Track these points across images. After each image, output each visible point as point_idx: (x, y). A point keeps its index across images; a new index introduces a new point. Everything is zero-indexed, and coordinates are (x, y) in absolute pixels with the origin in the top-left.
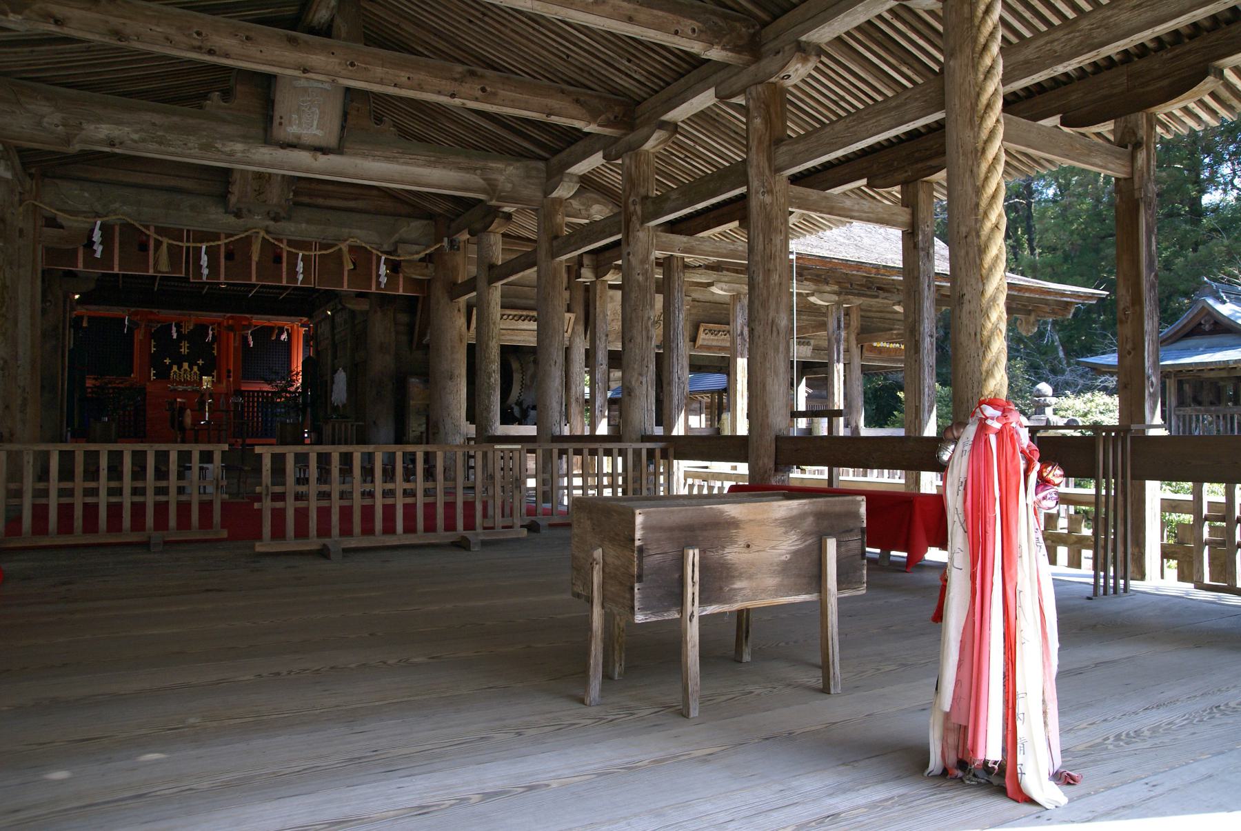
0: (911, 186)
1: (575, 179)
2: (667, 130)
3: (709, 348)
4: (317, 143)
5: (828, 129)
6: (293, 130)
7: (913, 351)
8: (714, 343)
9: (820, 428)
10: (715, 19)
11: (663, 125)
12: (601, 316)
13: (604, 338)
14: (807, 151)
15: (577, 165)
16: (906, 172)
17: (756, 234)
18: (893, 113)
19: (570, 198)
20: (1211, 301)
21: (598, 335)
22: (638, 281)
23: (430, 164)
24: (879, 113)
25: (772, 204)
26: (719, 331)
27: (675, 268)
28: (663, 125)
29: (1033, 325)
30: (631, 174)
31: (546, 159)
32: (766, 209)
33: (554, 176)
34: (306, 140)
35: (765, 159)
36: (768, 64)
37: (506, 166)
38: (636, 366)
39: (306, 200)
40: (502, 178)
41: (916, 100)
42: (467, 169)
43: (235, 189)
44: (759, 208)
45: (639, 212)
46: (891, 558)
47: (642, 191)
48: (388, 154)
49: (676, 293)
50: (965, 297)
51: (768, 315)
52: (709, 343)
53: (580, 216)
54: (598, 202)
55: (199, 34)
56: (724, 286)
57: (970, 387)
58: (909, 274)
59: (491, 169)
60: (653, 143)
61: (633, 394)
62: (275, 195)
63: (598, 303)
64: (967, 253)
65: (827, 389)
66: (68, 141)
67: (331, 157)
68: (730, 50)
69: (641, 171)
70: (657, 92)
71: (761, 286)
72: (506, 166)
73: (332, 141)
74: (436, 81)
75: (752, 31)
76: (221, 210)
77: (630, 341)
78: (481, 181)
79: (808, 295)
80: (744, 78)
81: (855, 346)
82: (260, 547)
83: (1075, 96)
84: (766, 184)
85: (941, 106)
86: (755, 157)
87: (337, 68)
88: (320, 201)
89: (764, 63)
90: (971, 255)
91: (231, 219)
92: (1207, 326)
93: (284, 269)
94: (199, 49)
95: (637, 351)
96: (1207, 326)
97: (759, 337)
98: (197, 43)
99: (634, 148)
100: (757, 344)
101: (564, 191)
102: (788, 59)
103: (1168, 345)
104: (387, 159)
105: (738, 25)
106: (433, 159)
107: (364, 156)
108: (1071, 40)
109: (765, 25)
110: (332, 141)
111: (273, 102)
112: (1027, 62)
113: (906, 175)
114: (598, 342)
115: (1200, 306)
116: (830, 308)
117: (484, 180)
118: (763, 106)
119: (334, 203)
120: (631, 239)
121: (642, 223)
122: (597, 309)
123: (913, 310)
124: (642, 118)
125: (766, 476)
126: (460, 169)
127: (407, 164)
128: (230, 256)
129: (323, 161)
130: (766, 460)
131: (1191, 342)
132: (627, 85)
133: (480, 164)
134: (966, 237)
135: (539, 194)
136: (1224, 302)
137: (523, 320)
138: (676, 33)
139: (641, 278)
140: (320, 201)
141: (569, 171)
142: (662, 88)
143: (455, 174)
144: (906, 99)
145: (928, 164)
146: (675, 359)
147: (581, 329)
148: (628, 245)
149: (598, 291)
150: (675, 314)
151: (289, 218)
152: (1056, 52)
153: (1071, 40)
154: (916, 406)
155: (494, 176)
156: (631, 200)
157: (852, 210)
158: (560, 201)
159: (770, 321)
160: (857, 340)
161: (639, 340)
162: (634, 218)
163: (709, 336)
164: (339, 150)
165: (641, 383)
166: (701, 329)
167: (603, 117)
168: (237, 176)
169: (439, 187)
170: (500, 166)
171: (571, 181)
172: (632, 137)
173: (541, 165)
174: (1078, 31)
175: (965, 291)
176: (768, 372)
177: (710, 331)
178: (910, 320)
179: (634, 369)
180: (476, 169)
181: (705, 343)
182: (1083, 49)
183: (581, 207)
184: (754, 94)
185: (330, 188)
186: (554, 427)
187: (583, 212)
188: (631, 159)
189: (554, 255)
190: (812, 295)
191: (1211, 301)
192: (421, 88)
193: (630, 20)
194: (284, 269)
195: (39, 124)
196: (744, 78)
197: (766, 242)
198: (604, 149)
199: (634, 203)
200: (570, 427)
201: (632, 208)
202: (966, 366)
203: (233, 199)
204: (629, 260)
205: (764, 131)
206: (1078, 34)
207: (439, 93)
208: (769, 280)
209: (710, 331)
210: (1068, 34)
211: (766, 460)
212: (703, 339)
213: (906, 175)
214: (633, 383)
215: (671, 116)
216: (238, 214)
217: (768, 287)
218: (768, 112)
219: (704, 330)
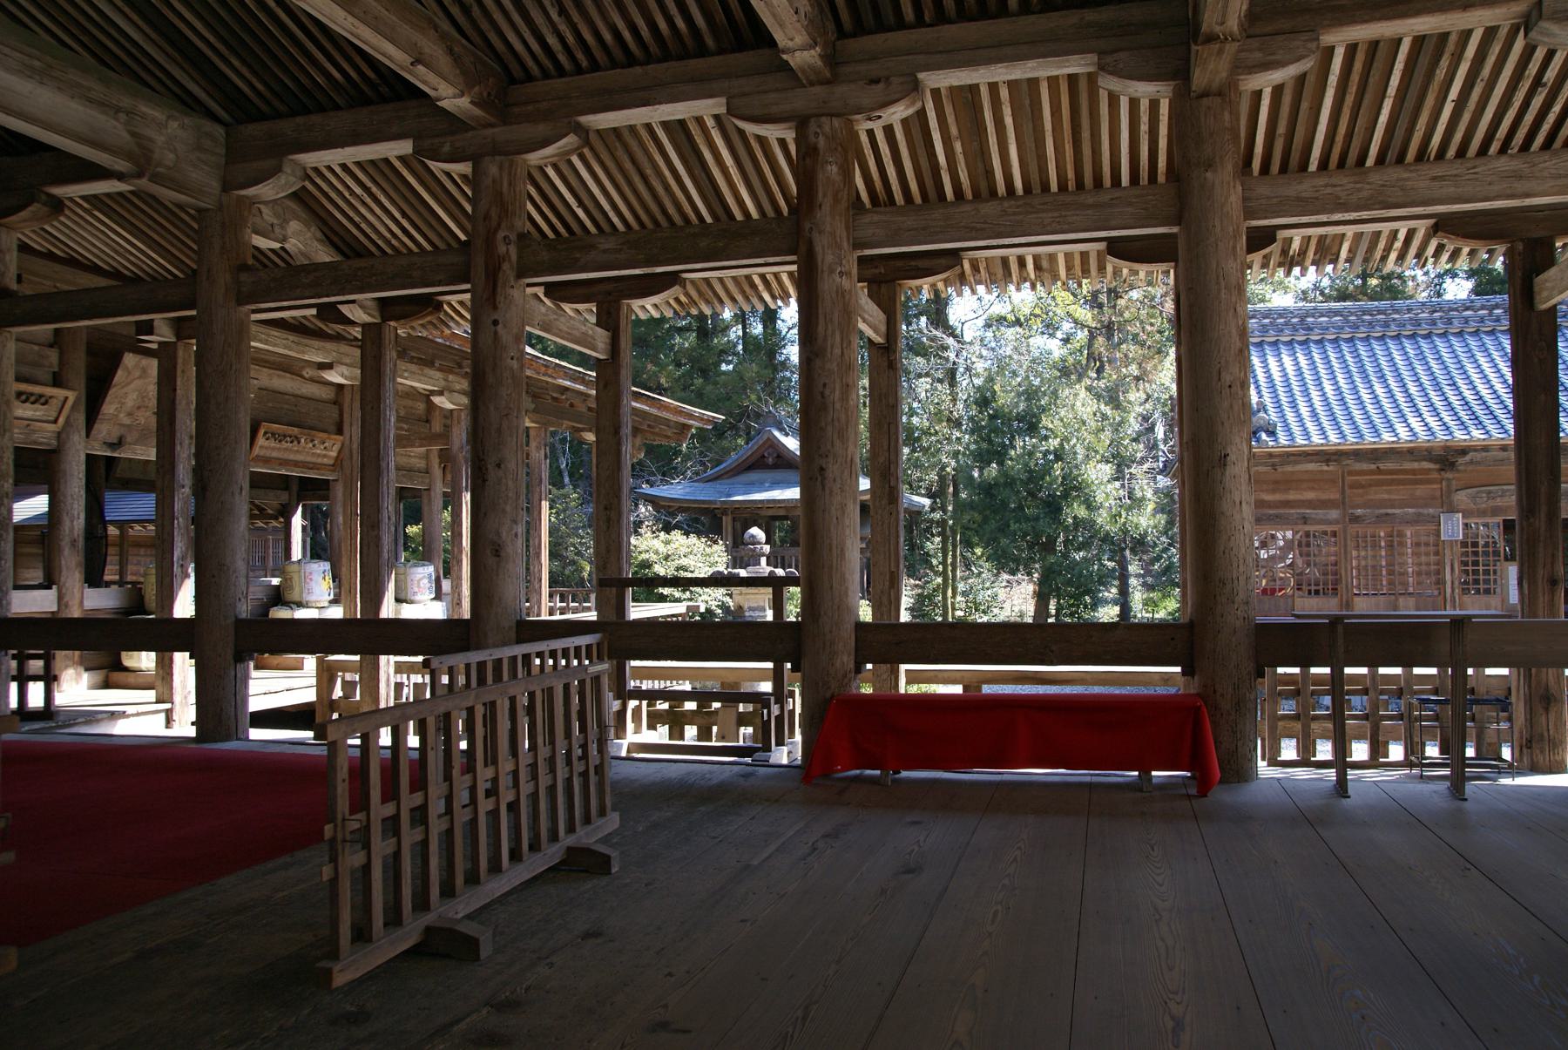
0: (884, 288)
2: (579, 137)
3: (266, 461)
5: (967, 208)
7: (884, 502)
8: (275, 454)
9: (409, 580)
12: (184, 402)
13: (187, 442)
14: (924, 229)
15: (323, 152)
16: (876, 267)
17: (829, 332)
18: (1089, 212)
20: (777, 433)
21: (178, 435)
22: (512, 369)
23: (28, 72)
26: (285, 436)
27: (387, 342)
29: (639, 449)
30: (501, 194)
32: (844, 297)
35: (843, 225)
37: (169, 117)
38: (508, 508)
40: (160, 139)
41: (1130, 204)
42: (102, 105)
44: (834, 295)
45: (514, 257)
46: (1154, 780)
49: (387, 384)
50: (1229, 458)
51: (846, 450)
52: (268, 453)
53: (272, 235)
54: (298, 218)
56: (344, 369)
57: (1235, 565)
58: (880, 400)
59: (144, 116)
61: (503, 554)
63: (179, 383)
69: (518, 189)
70: (561, 72)
71: (838, 406)
72: (169, 117)
77: (499, 466)
78: (125, 135)
79: (432, 393)
80: (800, 101)
81: (437, 466)
83: (1337, 242)
84: (844, 262)
85: (1178, 221)
86: (828, 219)
89: (840, 90)
90: (1236, 408)
92: (770, 460)
95: (510, 483)
96: (770, 460)
97: (835, 480)
100: (831, 492)
102: (897, 96)
103: (728, 478)
106: (37, 63)
108: (1359, 190)
112: (1299, 199)
113: (877, 271)
114: (178, 448)
115: (765, 437)
116: (455, 414)
117: (133, 134)
118: (840, 148)
120: (500, 299)
122: (178, 391)
123: (886, 447)
124: (530, 108)
125: (846, 680)
126: (90, 101)
130: (845, 659)
131: (754, 476)
132: (518, 47)
133: (126, 102)
134: (1230, 386)
135: (215, 185)
136: (787, 435)
137: (24, 402)
143: (81, 108)
144: (1112, 199)
145: (913, 263)
146: (385, 488)
147: (81, 419)
148: (495, 308)
149: (180, 361)
150: (386, 415)
152: (1340, 199)
153: (1359, 190)
154: (892, 573)
155: (149, 132)
156: (501, 235)
159: (849, 459)
160: (440, 458)
161: (512, 465)
162: (506, 266)
163: (272, 444)
165: (516, 535)
166: (262, 431)
170: (157, 114)
172: (501, 133)
173: (219, 131)
174: (1368, 183)
175: (1229, 451)
176: (847, 532)
177: (273, 434)
178: (881, 460)
179: (504, 511)
180: (118, 110)
181: (262, 454)
182: (1374, 204)
183: (275, 222)
184: (827, 128)
186: (239, 605)
187: (277, 229)
188: (501, 168)
190: (441, 393)
191: (777, 433)
196: (800, 101)
197: (845, 345)
200: (58, 588)
201: (502, 249)
202: (1229, 540)
204: (496, 333)
205: (842, 186)
206: (1368, 187)
208: (847, 400)
209: (273, 434)
210: (1356, 183)
211: (845, 659)
212: (261, 447)
213: (877, 271)
214: (504, 534)
215: (586, 120)
217: (847, 410)
219: (265, 433)
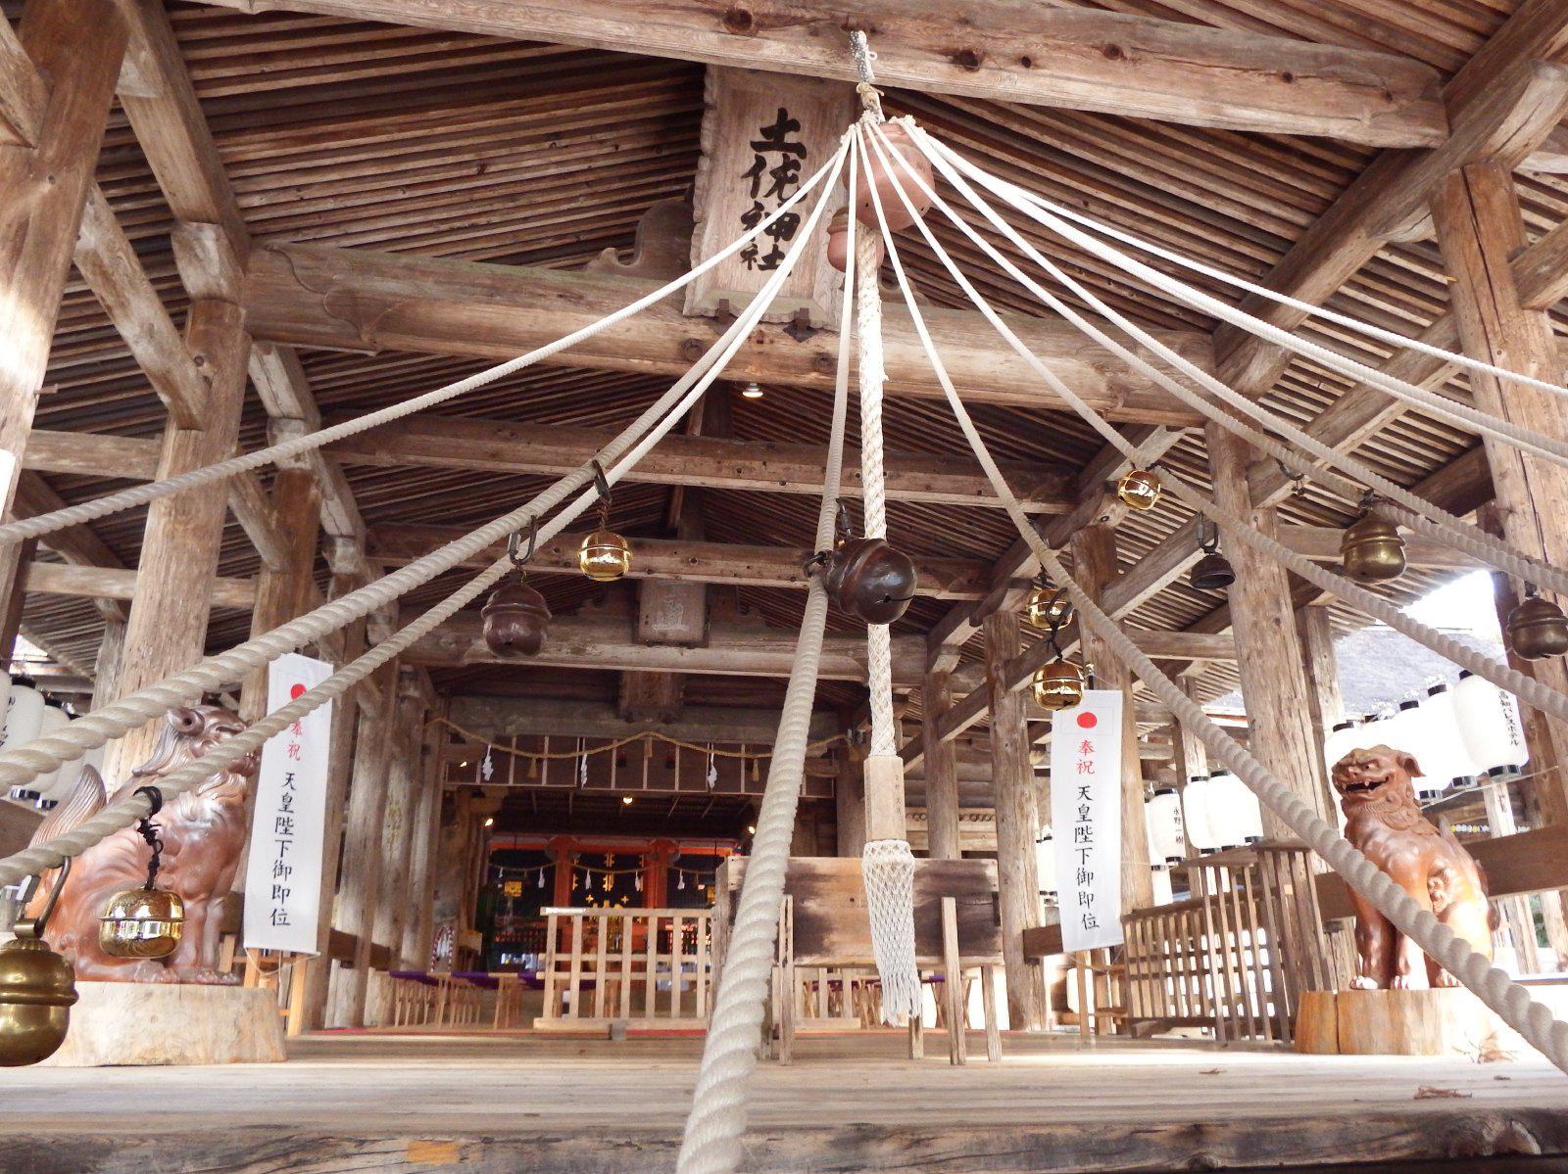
1: (954, 651)
4: (682, 637)
6: (658, 628)
10: (1022, 473)
11: (1016, 583)
19: (955, 671)
24: (1176, 544)
25: (1104, 651)
28: (1016, 583)
31: (926, 633)
33: (934, 648)
34: (671, 636)
36: (1086, 509)
39: (700, 699)
43: (626, 693)
47: (1004, 655)
48: (755, 642)
55: (557, 550)
60: (1010, 602)
62: (665, 697)
64: (1252, 676)
65: (1000, 821)
66: (459, 655)
67: (698, 651)
68: (1043, 501)
73: (697, 634)
74: (776, 567)
75: (1067, 478)
76: (612, 715)
82: (539, 1024)
87: (680, 566)
88: (714, 699)
91: (621, 723)
93: (677, 774)
94: (556, 563)
98: (555, 559)
99: (993, 609)
101: (946, 662)
104: (754, 648)
105: (1049, 475)
107: (731, 647)
109: (1080, 469)
110: (697, 634)
111: (638, 603)
119: (728, 700)
121: (1006, 691)
127: (774, 651)
128: (622, 762)
129: (689, 655)
138: (979, 493)
139: (1009, 749)
140: (714, 699)
141: (946, 642)
142: (1010, 545)
151: (679, 720)
157: (1215, 649)
158: (943, 676)
162: (998, 685)
164: (704, 643)
167: (955, 582)
168: (627, 679)
169: (757, 670)
171: (949, 653)
173: (920, 639)
185: (724, 684)
189: (939, 734)
192: (760, 576)
193: (928, 488)
194: (677, 774)
195: (437, 644)
198: (970, 615)
199: (997, 669)
203: (624, 704)
207: (779, 578)
216: (629, 719)
218: (1091, 556)
